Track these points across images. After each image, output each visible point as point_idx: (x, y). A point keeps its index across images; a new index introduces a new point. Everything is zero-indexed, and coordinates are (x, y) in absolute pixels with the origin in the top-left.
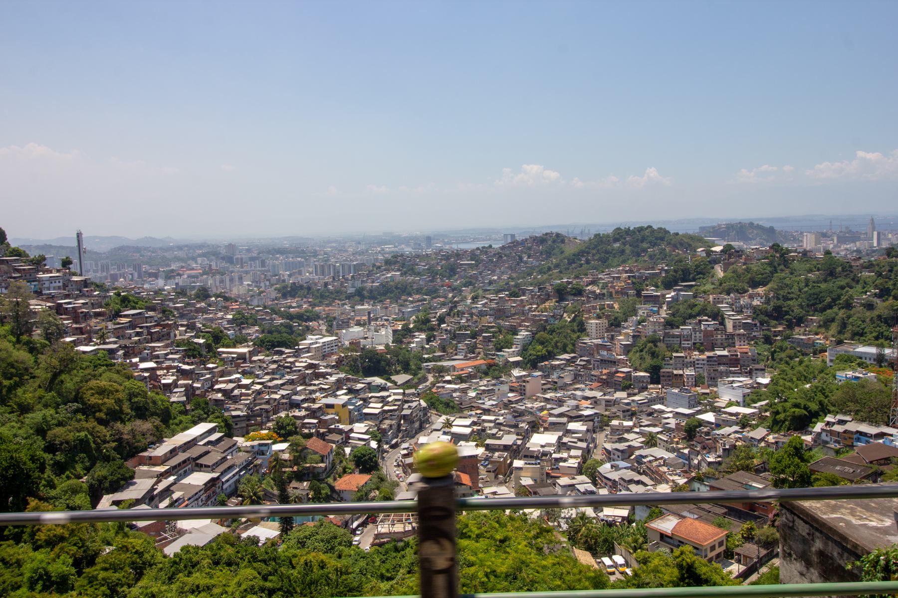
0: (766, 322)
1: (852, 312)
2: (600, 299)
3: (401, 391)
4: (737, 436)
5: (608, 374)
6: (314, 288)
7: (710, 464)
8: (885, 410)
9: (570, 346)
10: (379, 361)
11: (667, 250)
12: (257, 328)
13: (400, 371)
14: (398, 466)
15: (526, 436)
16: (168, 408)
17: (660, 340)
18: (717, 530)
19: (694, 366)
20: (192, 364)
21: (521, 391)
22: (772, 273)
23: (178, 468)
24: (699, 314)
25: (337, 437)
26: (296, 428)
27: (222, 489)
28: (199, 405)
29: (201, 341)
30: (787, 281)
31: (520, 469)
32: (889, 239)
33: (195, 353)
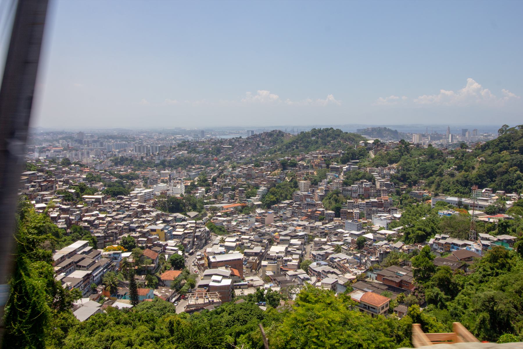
0: (398, 183)
1: (443, 178)
2: (306, 169)
3: (194, 221)
4: (387, 246)
5: (312, 212)
6: (135, 160)
7: (372, 262)
8: (467, 231)
9: (289, 196)
10: (178, 204)
11: (341, 142)
12: (101, 183)
13: (191, 210)
14: (195, 265)
15: (267, 247)
16: (57, 231)
17: (340, 193)
18: (385, 298)
19: (359, 207)
20: (68, 205)
21: (262, 222)
22: (400, 156)
23: (66, 268)
24: (361, 178)
25: (159, 249)
26: (135, 243)
27: (93, 280)
28: (77, 230)
29: (73, 191)
30: (408, 161)
31: (266, 266)
32: (457, 139)
33: (70, 198)
